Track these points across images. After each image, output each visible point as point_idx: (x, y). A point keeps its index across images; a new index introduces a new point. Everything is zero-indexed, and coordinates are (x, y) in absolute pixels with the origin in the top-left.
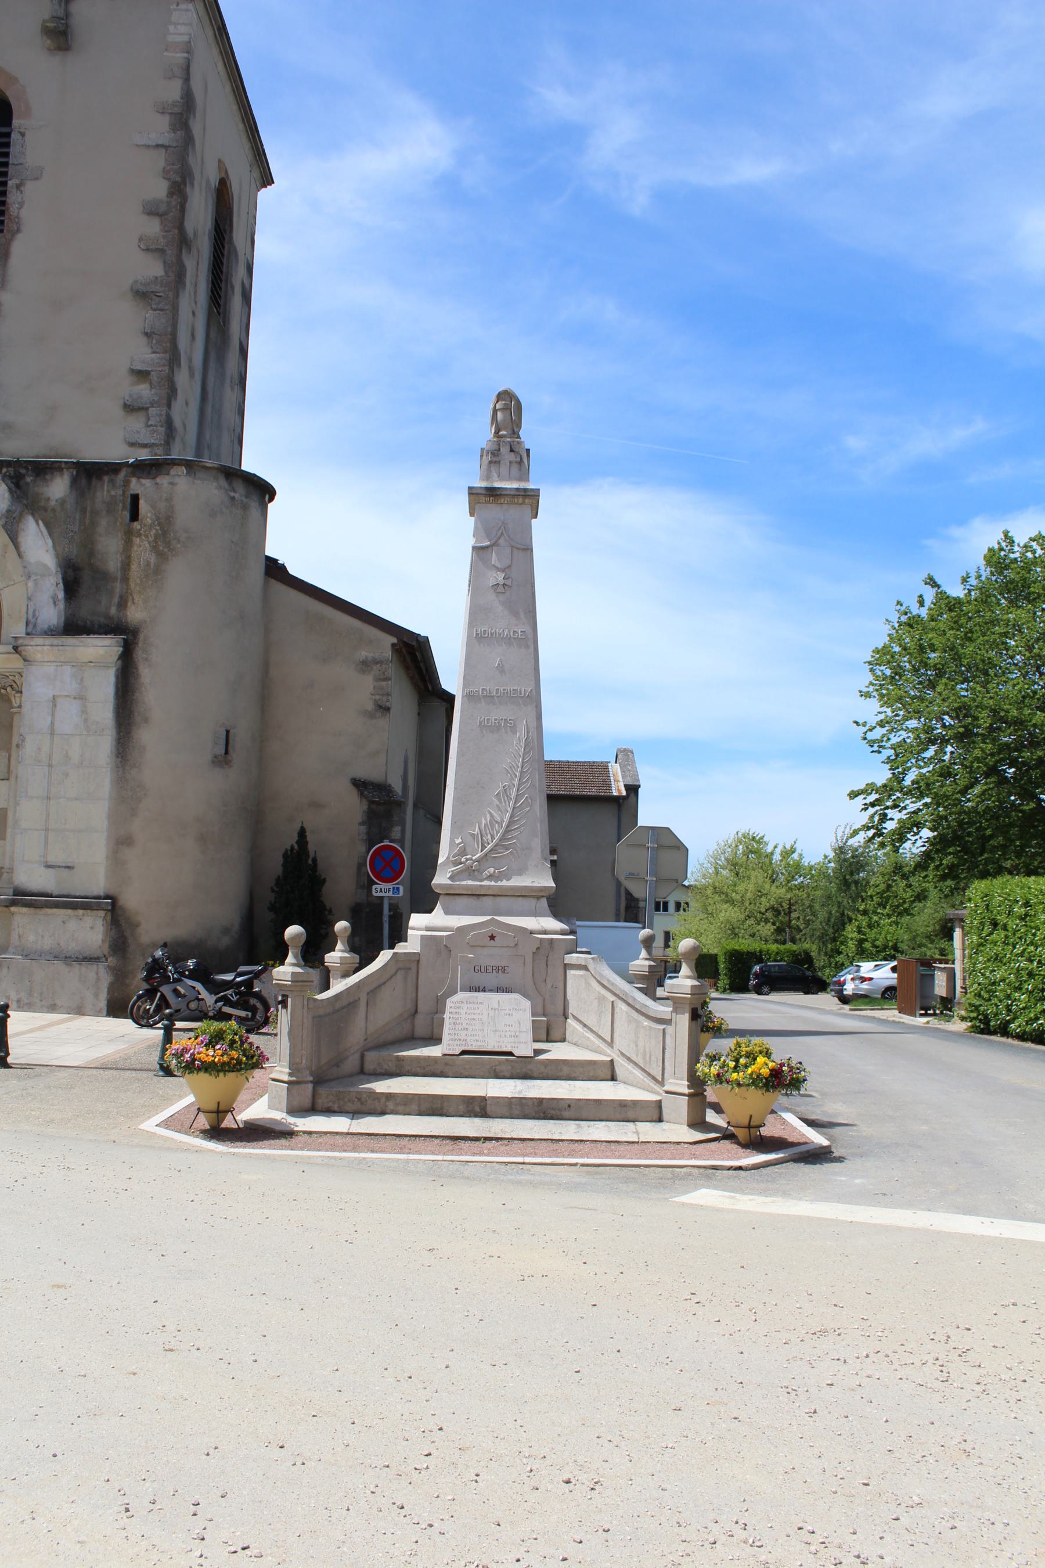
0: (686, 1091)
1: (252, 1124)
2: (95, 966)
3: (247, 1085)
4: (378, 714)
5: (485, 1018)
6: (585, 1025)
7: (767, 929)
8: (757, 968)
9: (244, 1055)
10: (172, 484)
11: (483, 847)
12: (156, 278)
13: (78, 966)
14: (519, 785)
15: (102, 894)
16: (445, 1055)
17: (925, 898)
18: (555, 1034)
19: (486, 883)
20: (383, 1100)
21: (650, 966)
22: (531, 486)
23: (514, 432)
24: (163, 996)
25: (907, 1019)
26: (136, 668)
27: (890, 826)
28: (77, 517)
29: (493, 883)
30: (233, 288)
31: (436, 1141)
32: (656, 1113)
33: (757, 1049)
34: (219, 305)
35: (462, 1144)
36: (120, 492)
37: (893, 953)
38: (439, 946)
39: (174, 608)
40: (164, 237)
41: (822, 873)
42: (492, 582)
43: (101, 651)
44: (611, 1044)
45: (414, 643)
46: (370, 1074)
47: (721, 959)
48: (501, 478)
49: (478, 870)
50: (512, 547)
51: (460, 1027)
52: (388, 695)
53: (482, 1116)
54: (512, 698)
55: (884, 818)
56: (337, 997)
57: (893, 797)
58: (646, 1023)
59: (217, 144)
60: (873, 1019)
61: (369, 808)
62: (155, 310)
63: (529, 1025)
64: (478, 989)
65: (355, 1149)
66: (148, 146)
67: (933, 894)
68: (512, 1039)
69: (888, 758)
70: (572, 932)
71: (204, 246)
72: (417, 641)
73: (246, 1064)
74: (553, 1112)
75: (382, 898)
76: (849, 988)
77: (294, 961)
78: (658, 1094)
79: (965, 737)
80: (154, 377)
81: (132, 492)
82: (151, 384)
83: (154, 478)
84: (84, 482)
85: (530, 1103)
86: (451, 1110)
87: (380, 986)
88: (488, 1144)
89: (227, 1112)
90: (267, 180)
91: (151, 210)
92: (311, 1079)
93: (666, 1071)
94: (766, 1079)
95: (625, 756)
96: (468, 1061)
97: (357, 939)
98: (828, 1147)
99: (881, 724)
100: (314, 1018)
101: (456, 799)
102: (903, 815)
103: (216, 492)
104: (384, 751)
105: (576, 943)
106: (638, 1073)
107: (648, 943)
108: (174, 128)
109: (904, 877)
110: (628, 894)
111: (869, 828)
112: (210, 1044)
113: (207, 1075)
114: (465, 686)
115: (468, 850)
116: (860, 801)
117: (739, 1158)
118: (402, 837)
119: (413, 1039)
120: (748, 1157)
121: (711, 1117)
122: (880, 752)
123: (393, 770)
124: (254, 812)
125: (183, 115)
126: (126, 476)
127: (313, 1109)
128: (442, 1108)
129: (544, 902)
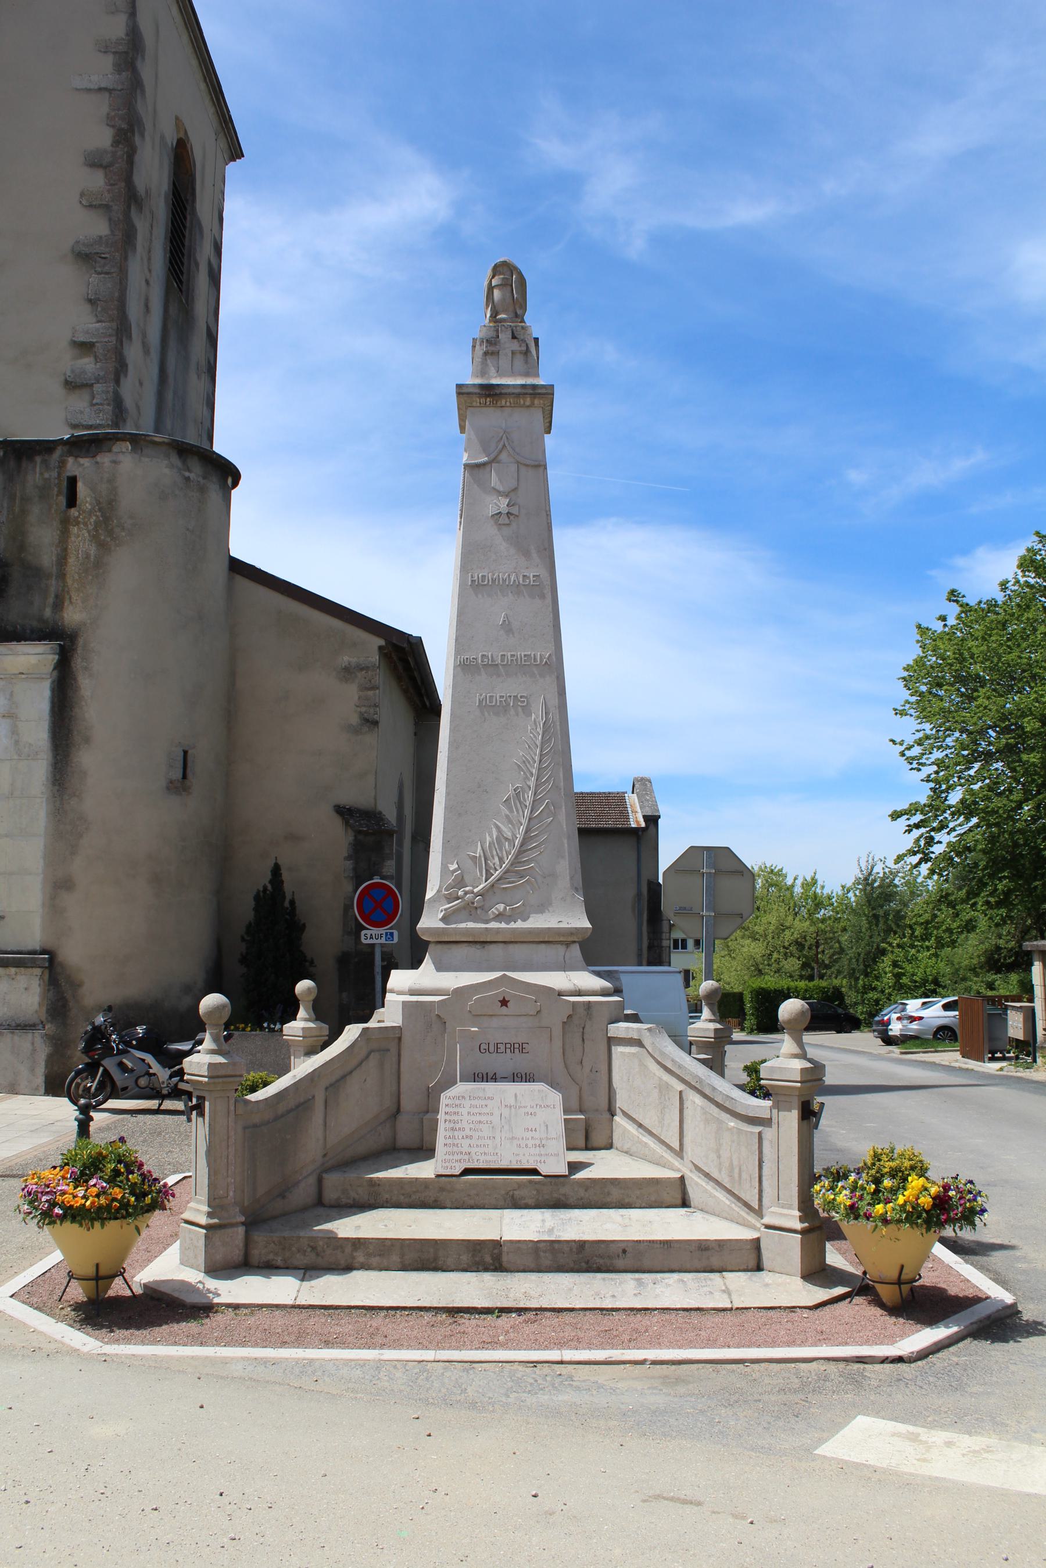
1: (155, 1291)
2: (30, 1035)
3: (140, 1239)
4: (365, 729)
5: (496, 1119)
6: (640, 1126)
7: (792, 964)
9: (132, 1193)
10: (115, 462)
11: (489, 875)
12: (101, 237)
13: (10, 1035)
15: (38, 948)
16: (438, 1176)
17: (974, 928)
18: (597, 1139)
19: (494, 925)
20: (348, 1249)
21: (716, 1030)
22: (540, 381)
23: (517, 316)
24: (106, 1072)
25: (972, 1064)
26: (75, 679)
27: (938, 850)
28: (5, 505)
29: (503, 925)
30: (197, 265)
31: (427, 1317)
33: (907, 1164)
34: (181, 282)
35: (469, 1323)
36: (55, 474)
37: (932, 987)
39: (118, 608)
40: (108, 191)
41: (844, 905)
42: (491, 510)
43: (33, 660)
44: (680, 1153)
45: (405, 645)
46: (332, 1206)
47: (747, 997)
48: (499, 373)
49: (482, 908)
50: (518, 462)
51: (461, 1134)
52: (376, 706)
53: (496, 1270)
54: (524, 667)
55: (930, 841)
57: (940, 818)
58: (733, 1123)
59: (170, 100)
60: (933, 1066)
61: (356, 839)
62: (99, 273)
63: (561, 1128)
65: (300, 1340)
66: (89, 90)
67: (983, 923)
68: (537, 1150)
69: (929, 776)
70: (617, 991)
71: (160, 208)
72: (409, 642)
73: (135, 1207)
74: (601, 1261)
75: (373, 945)
76: (896, 1028)
77: (213, 1046)
78: (754, 1228)
79: (1009, 752)
80: (99, 349)
81: (69, 474)
82: (96, 357)
83: (94, 456)
84: (12, 464)
85: (566, 1249)
86: (450, 1261)
87: (343, 1077)
88: (505, 1321)
89: (113, 1276)
90: (236, 152)
91: (94, 161)
92: (243, 1219)
93: (765, 1194)
94: (927, 1212)
95: (642, 785)
96: (473, 1185)
97: (344, 995)
98: (1014, 1305)
99: (919, 743)
100: (245, 1128)
101: (448, 809)
102: (952, 838)
103: (167, 471)
108: (118, 68)
109: (952, 905)
111: (915, 853)
112: (80, 1179)
113: (76, 1226)
115: (467, 879)
116: (903, 822)
117: (892, 1340)
120: (903, 1336)
122: (919, 770)
124: (219, 848)
125: (130, 53)
126: (61, 456)
127: (245, 1264)
128: (436, 1259)
129: (576, 951)
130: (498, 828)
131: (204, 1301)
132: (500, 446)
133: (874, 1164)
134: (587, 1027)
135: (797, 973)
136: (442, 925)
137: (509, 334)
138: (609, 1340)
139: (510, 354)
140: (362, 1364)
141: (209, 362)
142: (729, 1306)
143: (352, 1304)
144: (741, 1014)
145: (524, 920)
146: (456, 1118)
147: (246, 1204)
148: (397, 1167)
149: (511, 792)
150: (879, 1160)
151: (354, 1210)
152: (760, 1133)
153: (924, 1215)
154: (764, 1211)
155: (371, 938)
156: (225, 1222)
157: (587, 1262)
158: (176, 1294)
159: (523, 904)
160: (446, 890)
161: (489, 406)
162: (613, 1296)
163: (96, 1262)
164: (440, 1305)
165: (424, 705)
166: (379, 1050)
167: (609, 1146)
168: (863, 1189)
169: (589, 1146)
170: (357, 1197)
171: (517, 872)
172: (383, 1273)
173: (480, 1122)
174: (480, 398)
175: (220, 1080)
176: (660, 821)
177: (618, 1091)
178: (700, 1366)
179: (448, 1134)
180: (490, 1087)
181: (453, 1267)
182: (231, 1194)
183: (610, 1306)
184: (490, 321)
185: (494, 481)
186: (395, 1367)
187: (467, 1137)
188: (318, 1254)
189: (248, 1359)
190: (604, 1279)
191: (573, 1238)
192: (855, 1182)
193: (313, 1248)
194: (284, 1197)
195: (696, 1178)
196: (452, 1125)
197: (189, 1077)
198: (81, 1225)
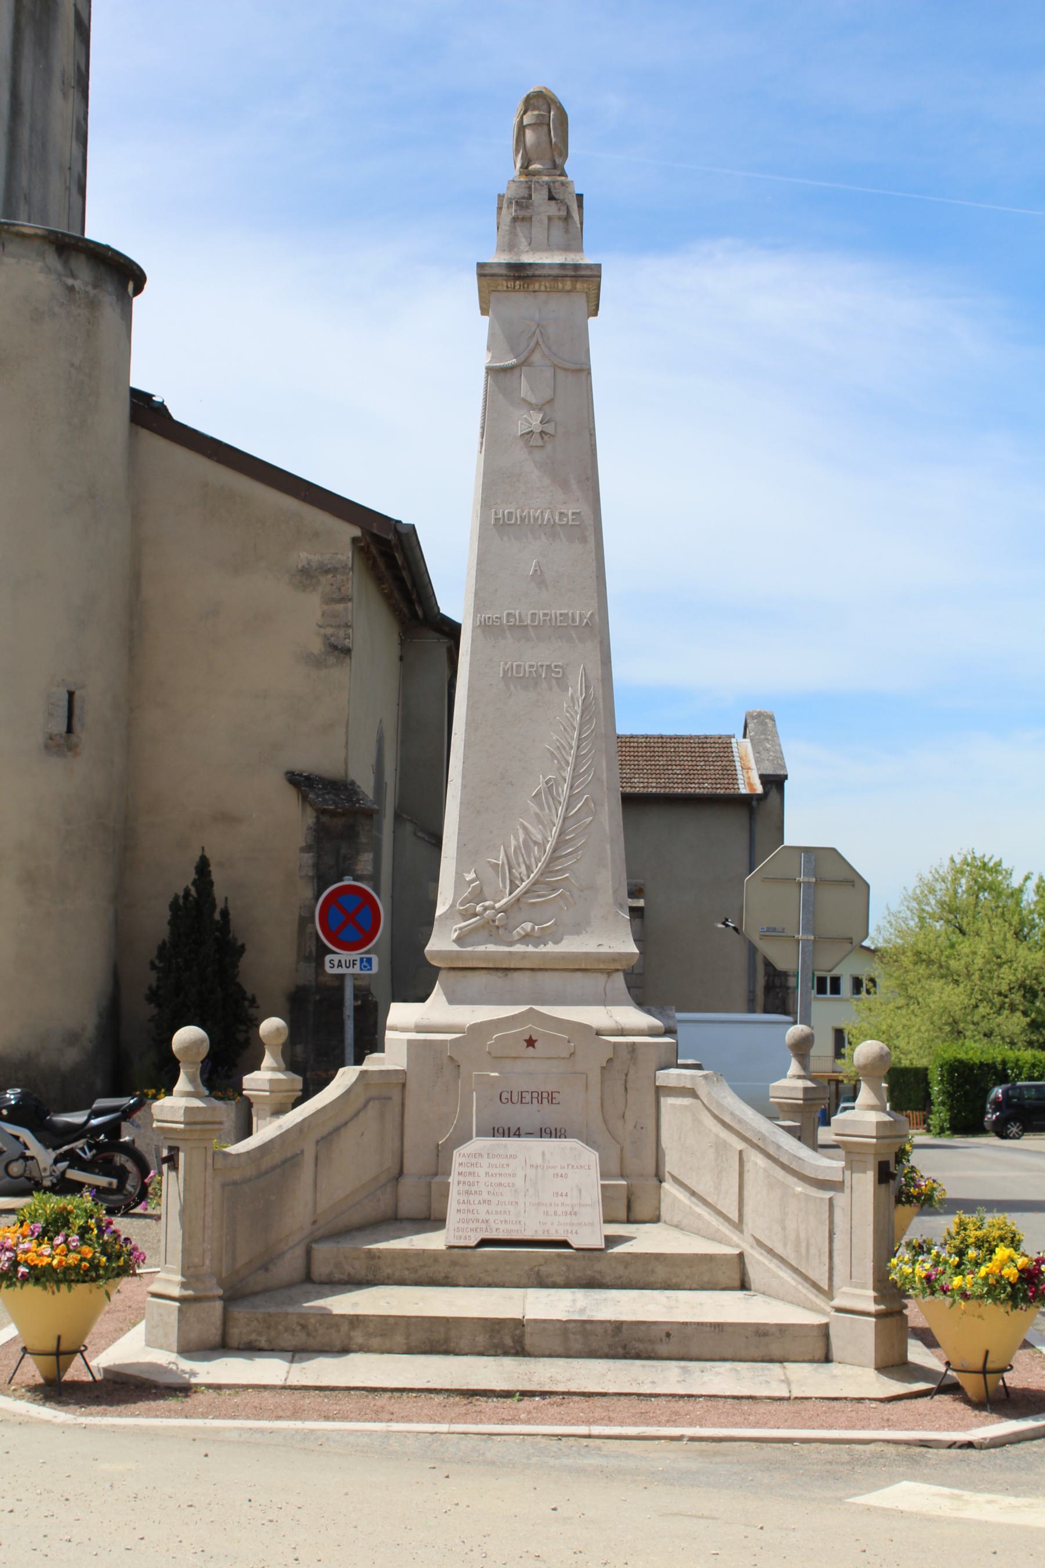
0: (872, 1307)
4: (332, 660)
5: (519, 1181)
6: (693, 1193)
7: (1015, 1023)
8: (998, 1092)
9: (104, 1253)
11: (513, 887)
14: (574, 778)
18: (641, 1209)
19: (519, 948)
20: (345, 1328)
21: (806, 1090)
22: (587, 258)
23: (555, 166)
29: (531, 949)
31: (438, 1399)
32: (821, 1348)
33: (996, 1233)
35: (482, 1403)
38: (435, 1056)
42: (521, 428)
44: (738, 1225)
45: (391, 537)
46: (322, 1283)
48: (533, 247)
49: (505, 927)
50: (555, 366)
52: (347, 626)
54: (560, 629)
56: (265, 1149)
58: (800, 1188)
63: (597, 1194)
64: (506, 1133)
65: (296, 1414)
70: (669, 1032)
72: (396, 531)
73: (106, 1268)
75: (341, 977)
77: (189, 1088)
78: (823, 1312)
86: (464, 1344)
87: (337, 1130)
88: (527, 1403)
89: (73, 1353)
92: (220, 1292)
93: (836, 1273)
94: (1012, 1285)
95: (760, 725)
97: (299, 1049)
101: (464, 804)
103: (41, 277)
104: (346, 729)
105: (675, 1050)
106: (786, 1275)
107: (802, 1048)
110: (768, 964)
114: (478, 608)
115: (487, 891)
117: (967, 1427)
118: (374, 871)
119: (396, 1221)
120: (983, 1424)
121: (917, 1353)
123: (360, 759)
124: (119, 833)
128: (447, 1340)
129: (619, 980)
130: (525, 828)
131: (180, 1381)
132: (532, 344)
133: (958, 1233)
134: (631, 1072)
135: (1023, 1037)
136: (456, 948)
137: (545, 194)
138: (644, 1419)
139: (546, 221)
140: (370, 1433)
141: (79, 68)
142: (787, 1395)
143: (352, 1385)
144: (925, 1104)
145: (556, 942)
146: (471, 1179)
147: (224, 1275)
148: (400, 1237)
149: (541, 785)
150: (965, 1229)
151: (349, 1287)
152: (831, 1199)
153: (1009, 1289)
154: (835, 1292)
155: (340, 965)
156: (201, 1294)
157: (624, 1347)
158: (146, 1376)
159: (555, 924)
160: (462, 904)
161: (519, 291)
162: (653, 1382)
163: (58, 1333)
164: (453, 1387)
165: (415, 615)
166: (379, 1099)
167: (656, 1219)
168: (946, 1262)
169: (632, 1219)
170: (352, 1271)
171: (548, 883)
172: (386, 1356)
173: (500, 1184)
174: (507, 281)
175: (198, 1127)
176: (786, 783)
177: (667, 1152)
178: (744, 1443)
179: (462, 1198)
180: (512, 1143)
181: (467, 1350)
182: (207, 1262)
183: (648, 1392)
184: (521, 174)
185: (525, 390)
186: (405, 1436)
187: (484, 1202)
188: (309, 1335)
189: (242, 1429)
190: (643, 1366)
191: (608, 1318)
192: (938, 1255)
193: (304, 1327)
194: (267, 1270)
195: (757, 1256)
196: (467, 1187)
197: (160, 1124)
198: (45, 1288)
